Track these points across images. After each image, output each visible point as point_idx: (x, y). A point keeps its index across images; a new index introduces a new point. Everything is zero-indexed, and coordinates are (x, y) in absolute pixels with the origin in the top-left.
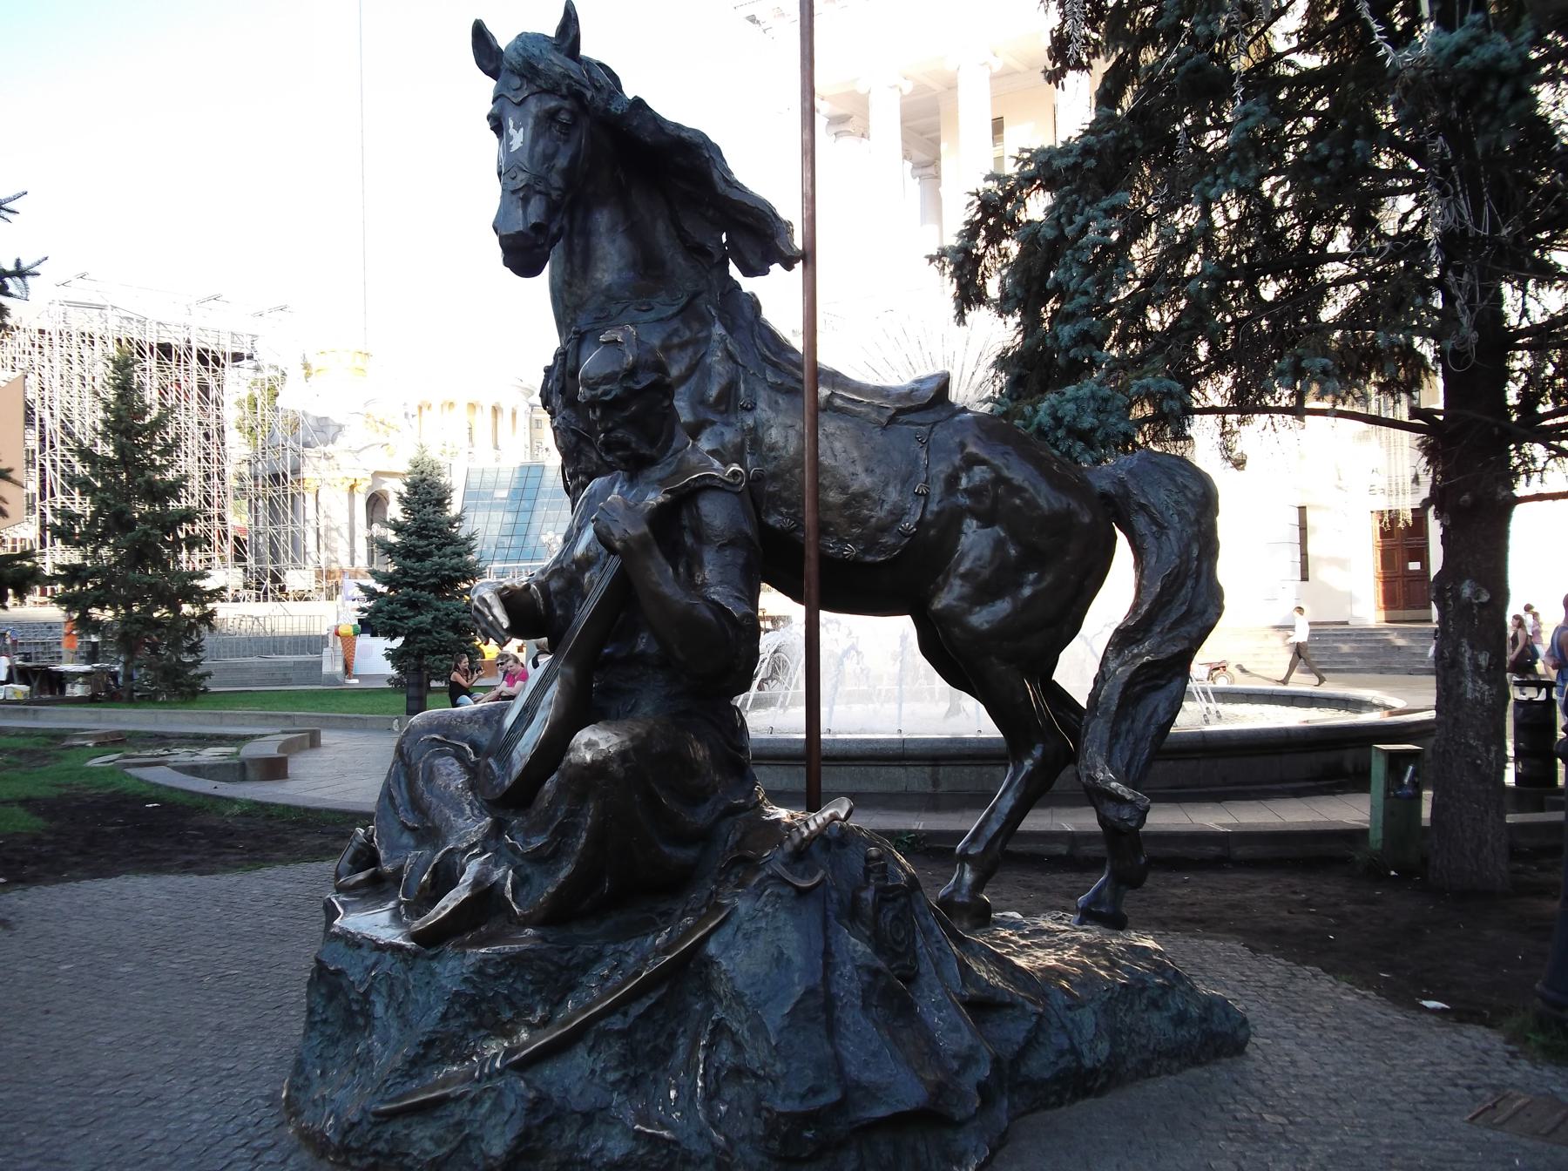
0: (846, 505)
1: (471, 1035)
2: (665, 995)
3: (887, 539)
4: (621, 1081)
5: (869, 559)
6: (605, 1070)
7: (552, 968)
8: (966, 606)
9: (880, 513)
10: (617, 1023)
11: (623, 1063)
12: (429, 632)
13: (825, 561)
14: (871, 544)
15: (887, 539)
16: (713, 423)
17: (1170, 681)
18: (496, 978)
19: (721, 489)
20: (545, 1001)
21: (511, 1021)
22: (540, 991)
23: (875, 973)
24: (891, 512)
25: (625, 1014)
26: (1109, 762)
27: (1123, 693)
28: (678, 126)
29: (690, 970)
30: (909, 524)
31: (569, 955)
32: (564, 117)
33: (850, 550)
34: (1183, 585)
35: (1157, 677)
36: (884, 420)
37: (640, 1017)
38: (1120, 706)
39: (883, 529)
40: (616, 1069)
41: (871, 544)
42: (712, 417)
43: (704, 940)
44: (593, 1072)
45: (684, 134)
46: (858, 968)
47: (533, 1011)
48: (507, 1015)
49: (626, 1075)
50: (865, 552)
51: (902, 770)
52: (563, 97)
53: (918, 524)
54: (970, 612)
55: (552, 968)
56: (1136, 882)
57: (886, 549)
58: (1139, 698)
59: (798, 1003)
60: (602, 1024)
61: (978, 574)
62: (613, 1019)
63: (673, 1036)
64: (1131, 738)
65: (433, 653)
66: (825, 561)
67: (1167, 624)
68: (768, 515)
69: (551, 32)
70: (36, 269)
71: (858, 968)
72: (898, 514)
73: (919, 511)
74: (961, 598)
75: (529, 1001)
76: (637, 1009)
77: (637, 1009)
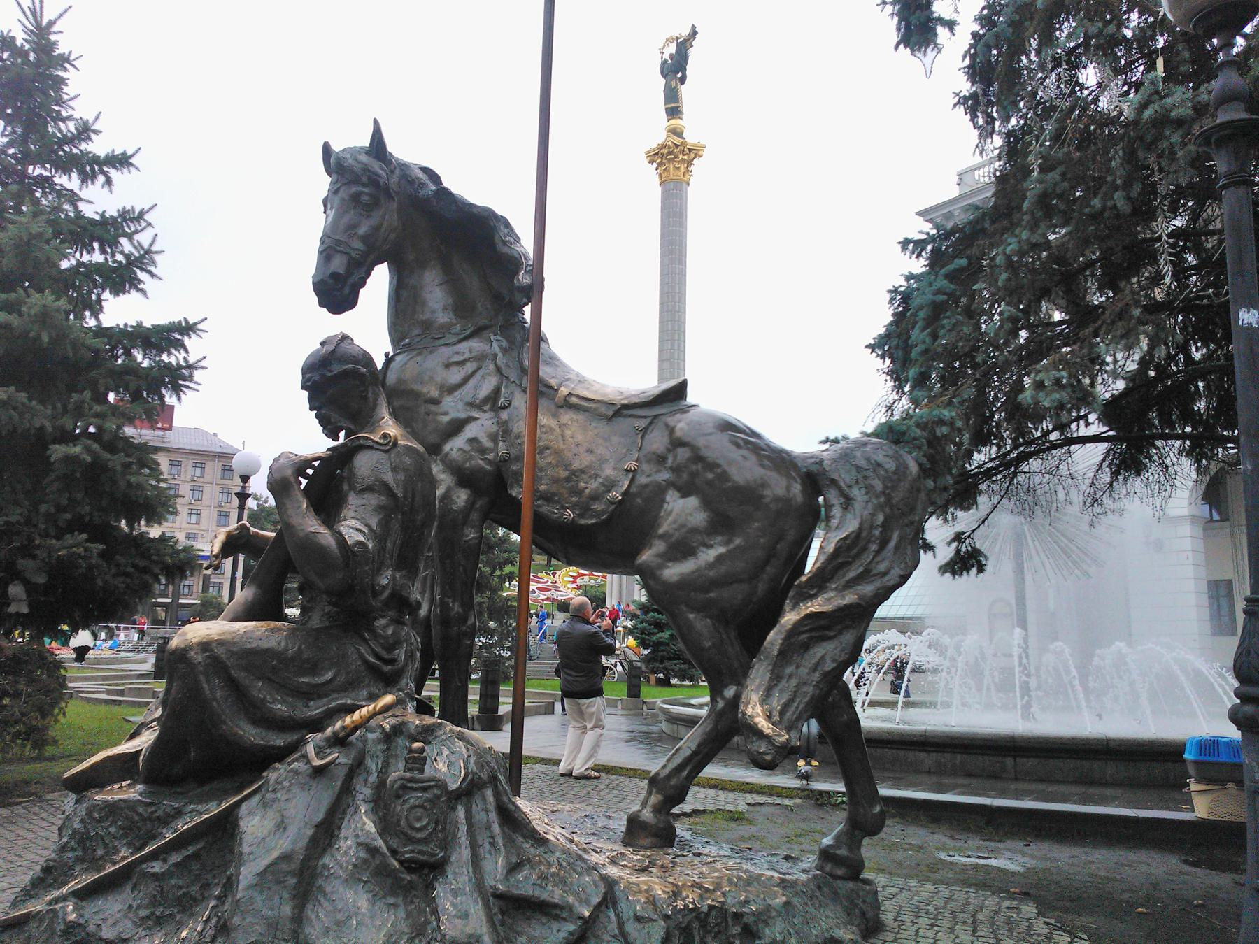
0: (568, 480)
1: (78, 868)
2: (200, 849)
3: (598, 506)
4: (148, 917)
5: (582, 522)
6: (139, 907)
7: (136, 818)
8: (660, 560)
9: (593, 485)
10: (157, 867)
11: (154, 903)
12: (668, 644)
13: (538, 519)
14: (585, 510)
15: (598, 506)
16: (477, 419)
17: (840, 632)
18: (98, 821)
19: (371, 448)
20: (129, 845)
21: (102, 857)
22: (125, 836)
23: (373, 851)
24: (602, 484)
25: (165, 861)
26: (763, 701)
27: (785, 639)
28: (471, 205)
29: (223, 830)
30: (616, 494)
31: (153, 809)
32: (365, 198)
33: (569, 514)
34: (864, 549)
35: (828, 628)
36: (611, 413)
37: (176, 865)
38: (781, 652)
39: (595, 497)
40: (146, 907)
41: (585, 510)
42: (475, 414)
43: (238, 804)
44: (130, 906)
45: (474, 210)
46: (359, 844)
47: (117, 852)
48: (100, 852)
49: (153, 913)
50: (582, 516)
51: (925, 754)
52: (364, 185)
53: (624, 494)
54: (662, 567)
55: (136, 818)
56: (874, 830)
57: (597, 514)
58: (806, 647)
59: (271, 865)
60: (144, 866)
61: (671, 536)
62: (153, 864)
63: (206, 886)
64: (794, 682)
65: (671, 659)
66: (538, 519)
67: (843, 581)
68: (512, 487)
69: (367, 143)
70: (201, 364)
71: (359, 844)
72: (610, 485)
73: (626, 484)
74: (658, 555)
75: (116, 843)
76: (175, 858)
77: (175, 858)
